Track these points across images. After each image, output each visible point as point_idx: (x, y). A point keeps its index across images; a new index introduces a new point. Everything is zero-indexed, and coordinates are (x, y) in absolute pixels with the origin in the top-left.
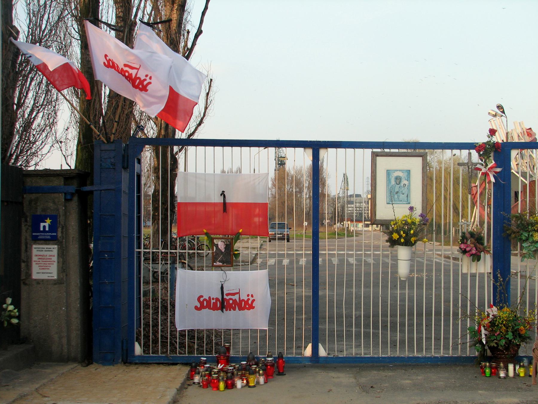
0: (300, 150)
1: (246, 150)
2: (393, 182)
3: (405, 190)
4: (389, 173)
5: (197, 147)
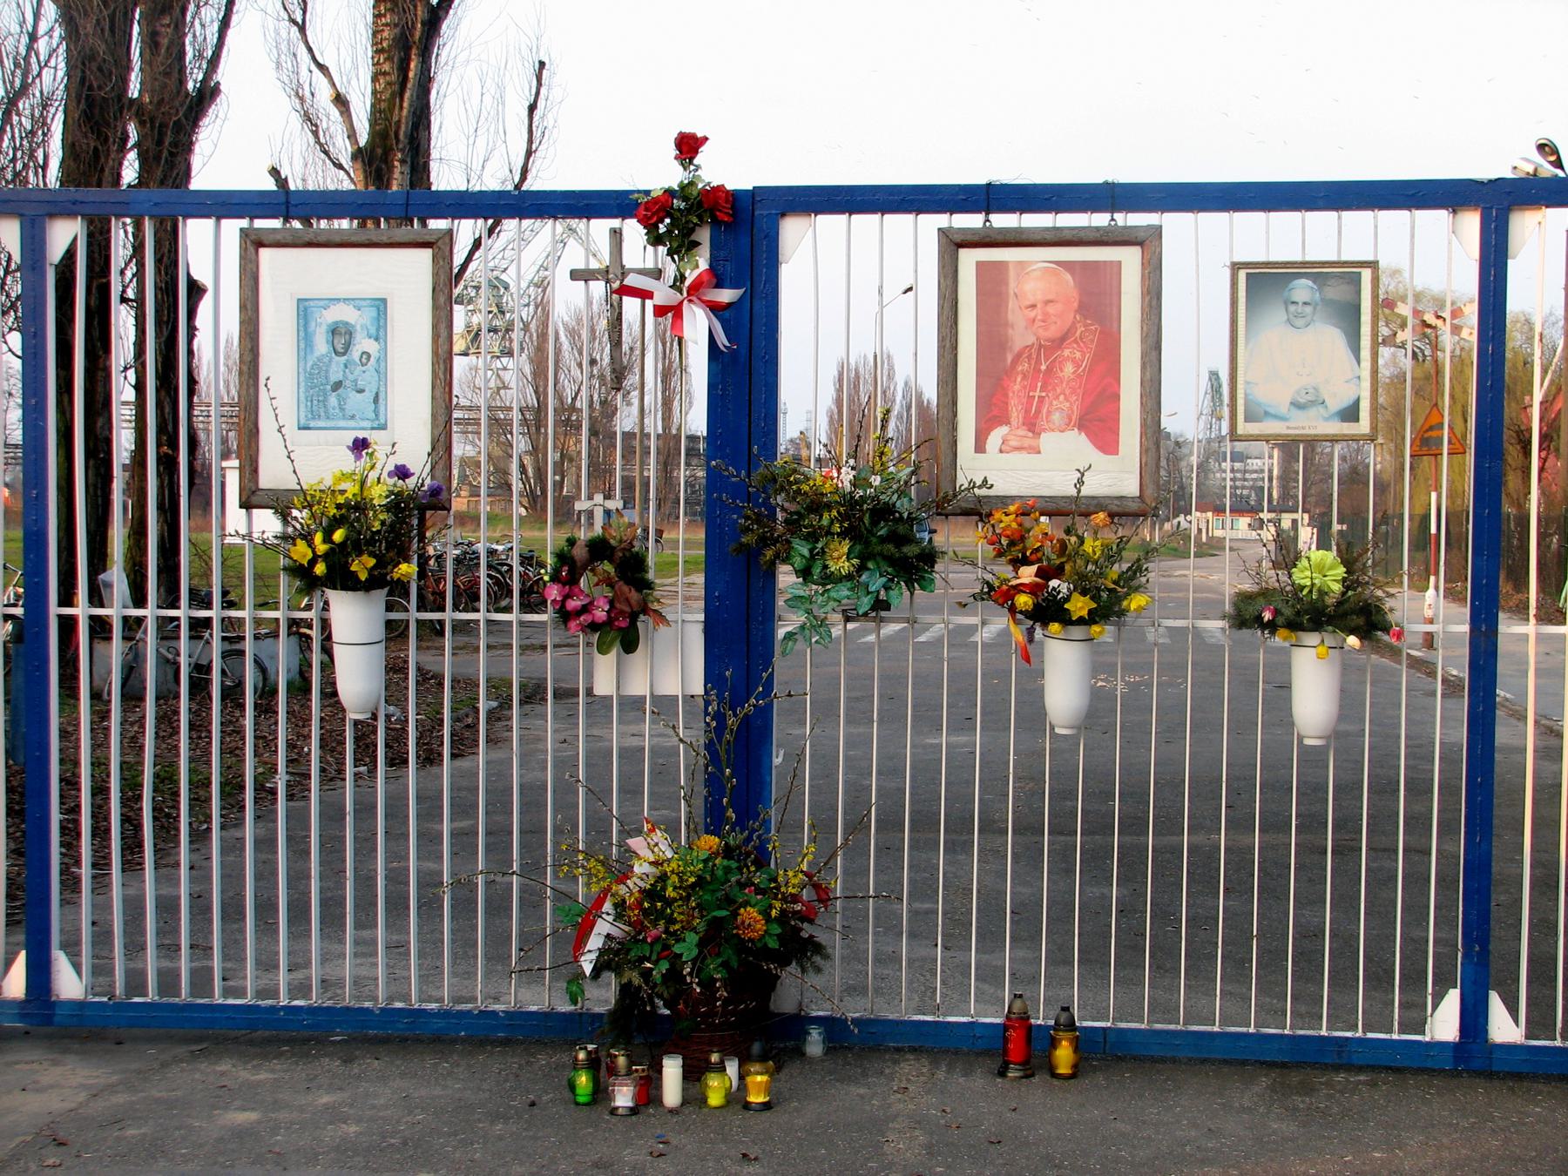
0: (1435, 220)
2: (321, 346)
3: (367, 378)
4: (305, 310)
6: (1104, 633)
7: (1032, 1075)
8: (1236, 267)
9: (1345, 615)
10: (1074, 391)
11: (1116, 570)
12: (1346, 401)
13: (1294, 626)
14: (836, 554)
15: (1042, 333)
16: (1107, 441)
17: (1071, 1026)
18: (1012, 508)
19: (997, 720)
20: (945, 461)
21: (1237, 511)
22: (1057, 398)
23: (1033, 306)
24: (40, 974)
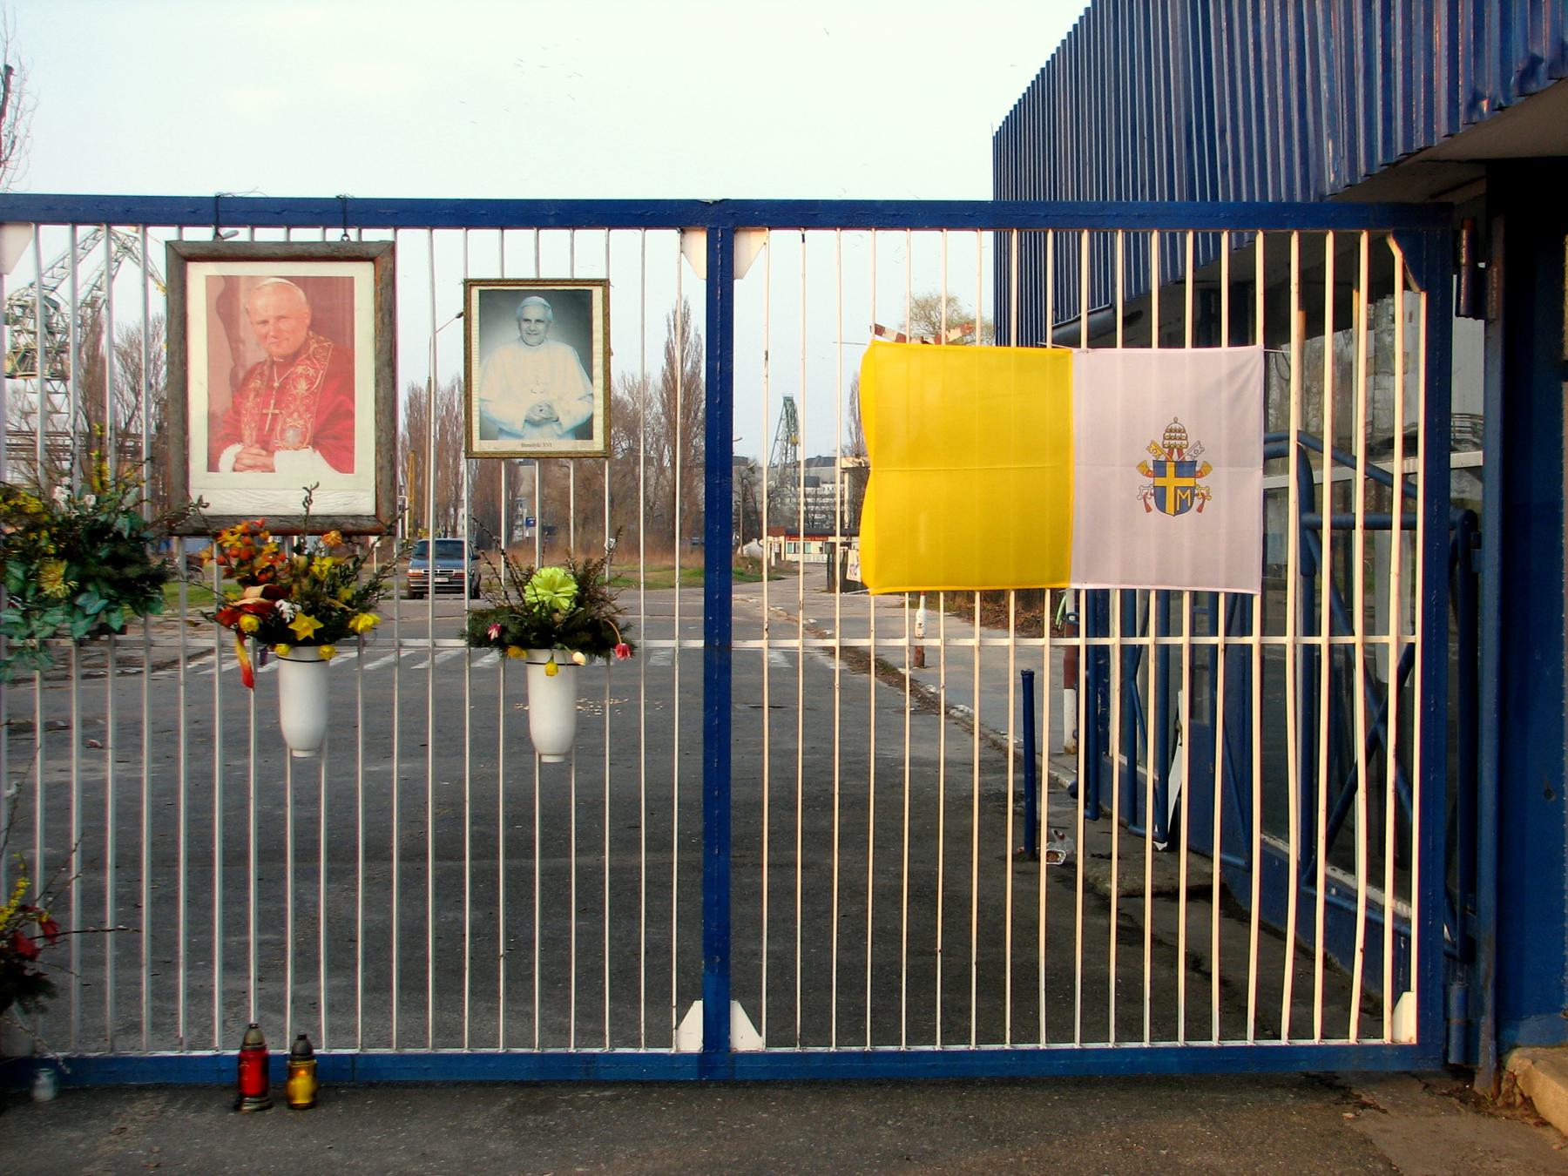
0: (666, 238)
1: (820, 238)
5: (435, 231)
6: (344, 655)
7: (269, 1107)
8: (469, 284)
9: (574, 631)
10: (308, 409)
11: (346, 593)
12: (580, 419)
13: (524, 643)
14: (51, 576)
15: (274, 349)
16: (341, 459)
17: (307, 1054)
18: (239, 527)
19: (484, 749)
20: (176, 479)
21: (810, 535)
22: (290, 416)
23: (265, 322)
24: (717, 1028)
